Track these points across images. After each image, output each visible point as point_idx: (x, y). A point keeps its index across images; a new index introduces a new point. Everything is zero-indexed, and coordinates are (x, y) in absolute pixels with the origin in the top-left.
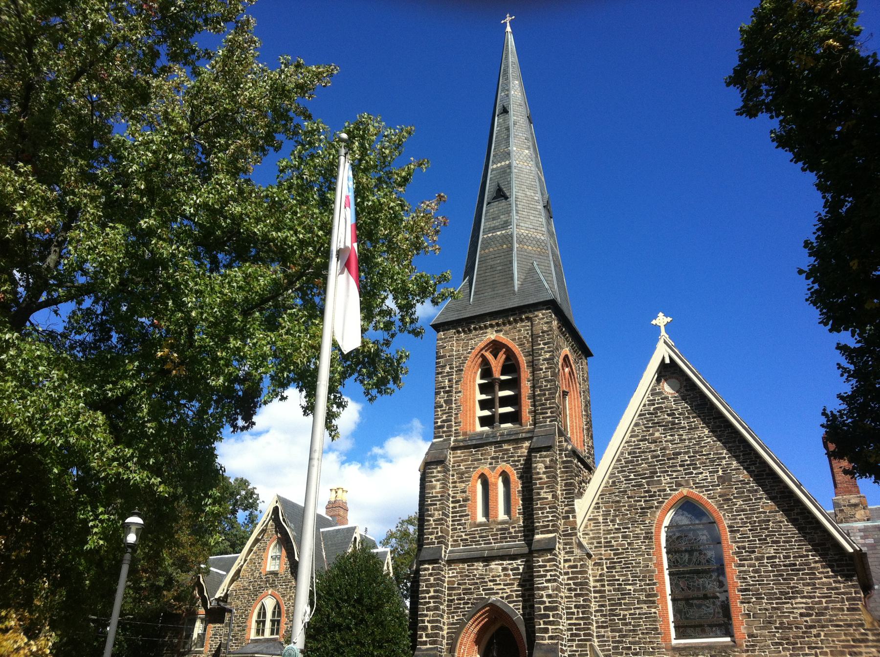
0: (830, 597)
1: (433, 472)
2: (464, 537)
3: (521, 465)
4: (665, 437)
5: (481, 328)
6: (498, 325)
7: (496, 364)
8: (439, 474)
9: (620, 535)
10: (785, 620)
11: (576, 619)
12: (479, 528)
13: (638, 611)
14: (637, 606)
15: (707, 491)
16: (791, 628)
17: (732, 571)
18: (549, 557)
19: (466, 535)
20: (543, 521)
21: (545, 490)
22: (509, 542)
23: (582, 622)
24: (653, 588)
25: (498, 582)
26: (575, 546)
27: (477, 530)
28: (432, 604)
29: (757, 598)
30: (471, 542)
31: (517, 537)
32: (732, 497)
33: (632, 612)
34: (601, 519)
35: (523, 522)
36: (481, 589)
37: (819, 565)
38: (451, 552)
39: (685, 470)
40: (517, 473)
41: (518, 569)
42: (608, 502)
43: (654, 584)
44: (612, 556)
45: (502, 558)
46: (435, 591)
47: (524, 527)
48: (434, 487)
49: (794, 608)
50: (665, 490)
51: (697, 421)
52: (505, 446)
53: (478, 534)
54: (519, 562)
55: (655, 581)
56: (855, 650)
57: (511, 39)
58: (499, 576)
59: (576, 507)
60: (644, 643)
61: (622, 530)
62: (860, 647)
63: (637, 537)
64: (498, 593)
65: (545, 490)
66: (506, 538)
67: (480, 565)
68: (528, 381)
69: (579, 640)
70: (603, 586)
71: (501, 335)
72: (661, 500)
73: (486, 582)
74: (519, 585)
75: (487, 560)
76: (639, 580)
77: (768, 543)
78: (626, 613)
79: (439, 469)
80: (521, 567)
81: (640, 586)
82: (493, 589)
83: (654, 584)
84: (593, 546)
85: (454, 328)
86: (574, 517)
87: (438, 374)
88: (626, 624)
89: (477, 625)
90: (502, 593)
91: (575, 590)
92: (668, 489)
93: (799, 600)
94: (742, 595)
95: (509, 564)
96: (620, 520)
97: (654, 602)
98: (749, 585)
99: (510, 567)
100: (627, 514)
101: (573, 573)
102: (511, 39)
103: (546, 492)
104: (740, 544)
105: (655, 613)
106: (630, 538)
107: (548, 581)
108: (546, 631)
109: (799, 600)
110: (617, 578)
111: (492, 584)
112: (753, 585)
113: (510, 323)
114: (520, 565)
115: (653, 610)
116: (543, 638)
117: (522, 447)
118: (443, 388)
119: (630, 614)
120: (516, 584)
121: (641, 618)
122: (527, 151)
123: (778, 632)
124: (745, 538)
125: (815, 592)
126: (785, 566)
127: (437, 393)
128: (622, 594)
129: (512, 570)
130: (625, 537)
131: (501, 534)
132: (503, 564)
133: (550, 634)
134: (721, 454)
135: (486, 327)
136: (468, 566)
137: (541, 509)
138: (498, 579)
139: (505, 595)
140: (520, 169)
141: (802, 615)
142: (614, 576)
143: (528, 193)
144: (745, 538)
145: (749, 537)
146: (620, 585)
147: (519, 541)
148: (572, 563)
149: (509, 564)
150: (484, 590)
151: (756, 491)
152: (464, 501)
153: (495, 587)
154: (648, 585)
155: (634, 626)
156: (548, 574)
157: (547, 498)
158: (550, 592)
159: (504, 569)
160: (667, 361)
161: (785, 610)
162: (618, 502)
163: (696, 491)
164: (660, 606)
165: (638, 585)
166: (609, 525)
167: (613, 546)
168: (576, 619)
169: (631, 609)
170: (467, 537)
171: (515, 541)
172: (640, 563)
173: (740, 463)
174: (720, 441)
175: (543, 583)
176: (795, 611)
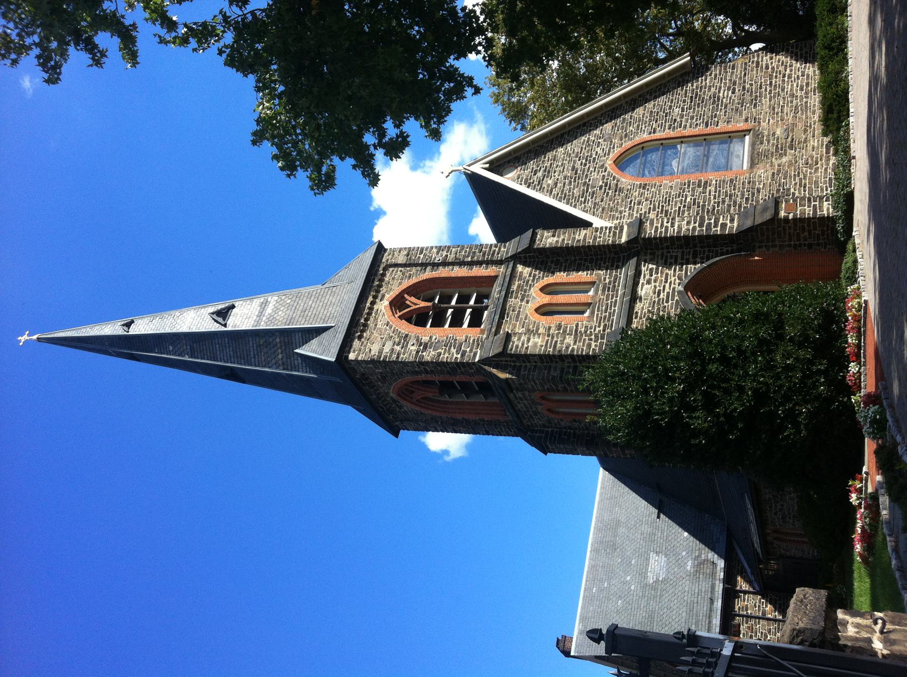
1: (517, 347)
3: (540, 273)
4: (555, 176)
5: (369, 314)
6: (375, 297)
7: (416, 303)
8: (522, 339)
10: (736, 101)
12: (596, 312)
13: (713, 193)
14: (707, 194)
15: (614, 148)
18: (648, 224)
19: (599, 327)
20: (609, 236)
22: (619, 284)
24: (693, 182)
25: (662, 288)
27: (597, 315)
29: (715, 117)
30: (608, 321)
31: (616, 276)
32: (625, 133)
33: (712, 197)
35: (602, 270)
36: (665, 304)
37: (695, 84)
39: (590, 163)
40: (547, 276)
41: (651, 270)
43: (689, 182)
44: (656, 212)
45: (635, 284)
47: (607, 270)
48: (535, 344)
49: (727, 96)
51: (550, 155)
52: (514, 287)
53: (601, 314)
54: (643, 269)
55: (686, 181)
56: (764, 67)
58: (655, 287)
60: (743, 188)
61: (632, 205)
62: (762, 64)
63: (642, 195)
66: (614, 286)
67: (638, 306)
68: (453, 269)
71: (387, 296)
72: (612, 178)
73: (659, 300)
74: (670, 269)
75: (634, 298)
76: (684, 192)
77: (670, 112)
78: (712, 202)
79: (516, 339)
80: (651, 266)
81: (689, 192)
82: (668, 293)
83: (689, 182)
85: (352, 341)
88: (724, 202)
90: (674, 284)
92: (603, 173)
94: (711, 125)
95: (644, 277)
96: (622, 207)
97: (706, 183)
98: (703, 122)
99: (647, 277)
100: (618, 202)
103: (579, 235)
104: (667, 127)
105: (716, 181)
106: (641, 200)
107: (672, 225)
108: (724, 226)
110: (677, 209)
111: (662, 294)
112: (704, 119)
113: (380, 286)
114: (648, 267)
115: (714, 182)
117: (521, 273)
119: (715, 198)
120: (667, 271)
121: (720, 191)
123: (745, 106)
124: (662, 125)
125: (716, 86)
128: (694, 204)
129: (651, 275)
131: (608, 291)
132: (643, 283)
133: (728, 222)
134: (584, 140)
135: (371, 309)
136: (636, 318)
137: (595, 238)
138: (658, 288)
139: (677, 281)
141: (733, 93)
142: (675, 211)
144: (662, 125)
145: (662, 123)
146: (684, 206)
147: (620, 274)
149: (644, 277)
150: (667, 302)
151: (624, 119)
152: (559, 329)
154: (689, 186)
155: (726, 196)
156: (665, 224)
157: (586, 234)
159: (649, 282)
160: (487, 165)
161: (728, 101)
162: (603, 209)
163: (611, 156)
164: (710, 178)
165: (688, 193)
166: (624, 215)
167: (645, 212)
169: (710, 198)
170: (602, 324)
171: (620, 277)
172: (667, 192)
173: (597, 128)
174: (573, 141)
175: (674, 229)
176: (729, 96)
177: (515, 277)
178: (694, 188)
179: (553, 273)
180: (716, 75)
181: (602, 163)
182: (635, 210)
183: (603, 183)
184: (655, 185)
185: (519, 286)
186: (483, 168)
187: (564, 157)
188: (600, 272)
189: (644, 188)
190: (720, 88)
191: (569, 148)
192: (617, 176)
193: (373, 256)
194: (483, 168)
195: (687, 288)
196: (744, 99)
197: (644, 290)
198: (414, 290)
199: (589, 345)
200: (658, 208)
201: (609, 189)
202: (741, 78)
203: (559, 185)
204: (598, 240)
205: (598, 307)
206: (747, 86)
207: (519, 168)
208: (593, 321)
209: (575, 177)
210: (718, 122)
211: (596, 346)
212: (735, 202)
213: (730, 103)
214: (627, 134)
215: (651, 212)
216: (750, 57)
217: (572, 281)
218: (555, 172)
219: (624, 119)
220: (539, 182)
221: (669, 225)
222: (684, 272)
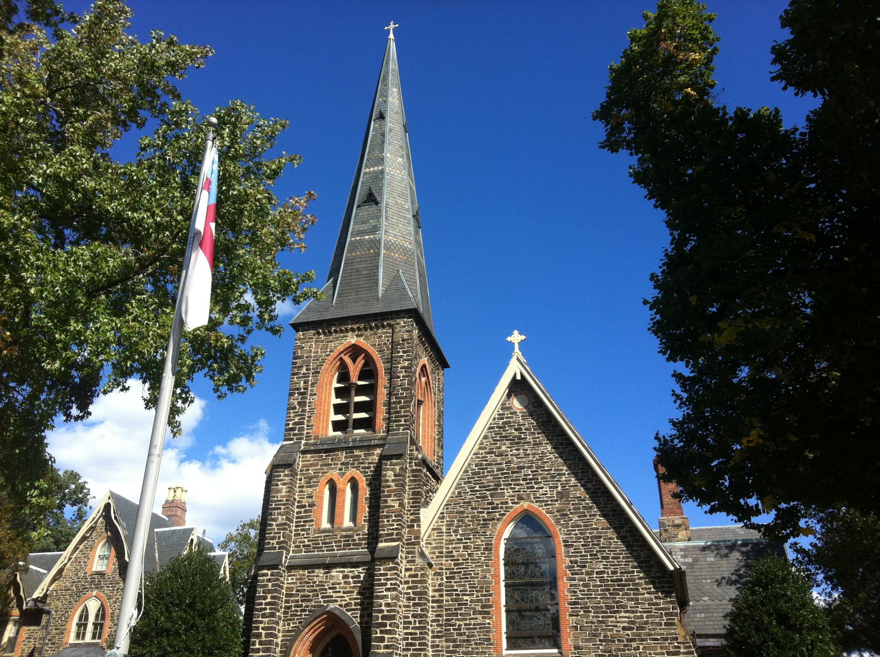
0: (651, 612)
2: (307, 543)
4: (511, 451)
5: (342, 332)
6: (359, 329)
9: (461, 546)
11: (413, 628)
12: (322, 535)
13: (472, 622)
14: (472, 616)
15: (546, 505)
16: (614, 641)
17: (564, 584)
18: (391, 565)
19: (308, 541)
21: (392, 498)
23: (418, 632)
25: (338, 590)
26: (417, 555)
27: (321, 537)
28: (268, 611)
29: (585, 612)
32: (569, 513)
33: (468, 622)
34: (444, 529)
35: (368, 530)
36: (320, 596)
37: (642, 581)
38: (292, 558)
39: (527, 484)
41: (359, 577)
42: (452, 512)
46: (272, 598)
48: (280, 491)
49: (618, 622)
50: (507, 503)
51: (541, 437)
52: (357, 453)
54: (360, 569)
55: (491, 592)
57: (393, 46)
58: (340, 583)
59: (421, 516)
61: (464, 541)
63: (477, 548)
64: (336, 601)
65: (392, 498)
66: (349, 545)
67: (320, 572)
69: (414, 650)
70: (442, 596)
71: (361, 339)
73: (326, 590)
74: (358, 594)
77: (598, 558)
82: (332, 597)
83: (491, 595)
84: (434, 556)
86: (419, 526)
87: (294, 374)
89: (315, 631)
90: (341, 601)
91: (414, 599)
92: (510, 502)
93: (623, 614)
94: (571, 608)
95: (350, 572)
96: (462, 531)
98: (579, 599)
99: (351, 574)
100: (470, 525)
101: (413, 582)
102: (393, 46)
103: (393, 500)
104: (573, 559)
105: (489, 624)
107: (388, 590)
108: (382, 639)
109: (623, 614)
110: (455, 588)
111: (331, 591)
113: (371, 328)
114: (362, 573)
115: (488, 621)
116: (378, 647)
117: (373, 454)
118: (298, 389)
119: (465, 625)
120: (356, 592)
121: (475, 629)
122: (401, 160)
123: (602, 645)
124: (577, 552)
125: (638, 607)
126: (612, 581)
127: (291, 394)
130: (465, 548)
132: (344, 571)
134: (562, 470)
135: (347, 331)
136: (308, 572)
139: (344, 603)
140: (392, 176)
141: (624, 628)
142: (453, 586)
143: (398, 201)
144: (577, 552)
146: (458, 595)
148: (413, 573)
149: (350, 572)
151: (591, 508)
153: (335, 595)
154: (485, 596)
155: (468, 636)
156: (389, 583)
158: (389, 601)
159: (345, 577)
160: (519, 377)
161: (610, 624)
162: (462, 512)
163: (535, 505)
164: (494, 617)
165: (475, 596)
168: (413, 628)
170: (310, 543)
172: (478, 574)
174: (561, 457)
175: (383, 592)
177: (368, 450)
178: (482, 602)
179: (368, 485)
180: (657, 604)
181: (524, 497)
182: (458, 545)
183: (498, 504)
184: (488, 560)
185: (359, 456)
186: (515, 374)
187: (538, 454)
188: (366, 528)
189: (486, 549)
190: (633, 612)
191: (551, 456)
192: (505, 517)
193: (364, 313)
194: (515, 374)
195: (331, 615)
196: (614, 641)
197: (337, 574)
198: (369, 361)
199: (273, 538)
200: (457, 569)
201: (488, 513)
202: (650, 635)
203: (499, 459)
204: (385, 520)
205: (328, 536)
206: (634, 644)
207: (524, 410)
208: (315, 534)
209: (508, 473)
210: (577, 615)
211: (273, 544)
212: (458, 646)
213: (608, 626)
214: (567, 515)
215: (452, 562)
216: (688, 643)
217: (359, 504)
218: (517, 450)
219: (591, 508)
220: (505, 437)
221: (389, 586)
222: (353, 607)
